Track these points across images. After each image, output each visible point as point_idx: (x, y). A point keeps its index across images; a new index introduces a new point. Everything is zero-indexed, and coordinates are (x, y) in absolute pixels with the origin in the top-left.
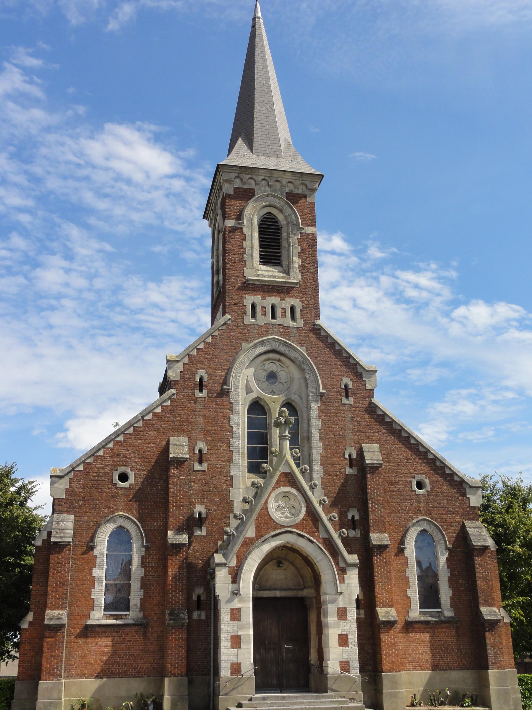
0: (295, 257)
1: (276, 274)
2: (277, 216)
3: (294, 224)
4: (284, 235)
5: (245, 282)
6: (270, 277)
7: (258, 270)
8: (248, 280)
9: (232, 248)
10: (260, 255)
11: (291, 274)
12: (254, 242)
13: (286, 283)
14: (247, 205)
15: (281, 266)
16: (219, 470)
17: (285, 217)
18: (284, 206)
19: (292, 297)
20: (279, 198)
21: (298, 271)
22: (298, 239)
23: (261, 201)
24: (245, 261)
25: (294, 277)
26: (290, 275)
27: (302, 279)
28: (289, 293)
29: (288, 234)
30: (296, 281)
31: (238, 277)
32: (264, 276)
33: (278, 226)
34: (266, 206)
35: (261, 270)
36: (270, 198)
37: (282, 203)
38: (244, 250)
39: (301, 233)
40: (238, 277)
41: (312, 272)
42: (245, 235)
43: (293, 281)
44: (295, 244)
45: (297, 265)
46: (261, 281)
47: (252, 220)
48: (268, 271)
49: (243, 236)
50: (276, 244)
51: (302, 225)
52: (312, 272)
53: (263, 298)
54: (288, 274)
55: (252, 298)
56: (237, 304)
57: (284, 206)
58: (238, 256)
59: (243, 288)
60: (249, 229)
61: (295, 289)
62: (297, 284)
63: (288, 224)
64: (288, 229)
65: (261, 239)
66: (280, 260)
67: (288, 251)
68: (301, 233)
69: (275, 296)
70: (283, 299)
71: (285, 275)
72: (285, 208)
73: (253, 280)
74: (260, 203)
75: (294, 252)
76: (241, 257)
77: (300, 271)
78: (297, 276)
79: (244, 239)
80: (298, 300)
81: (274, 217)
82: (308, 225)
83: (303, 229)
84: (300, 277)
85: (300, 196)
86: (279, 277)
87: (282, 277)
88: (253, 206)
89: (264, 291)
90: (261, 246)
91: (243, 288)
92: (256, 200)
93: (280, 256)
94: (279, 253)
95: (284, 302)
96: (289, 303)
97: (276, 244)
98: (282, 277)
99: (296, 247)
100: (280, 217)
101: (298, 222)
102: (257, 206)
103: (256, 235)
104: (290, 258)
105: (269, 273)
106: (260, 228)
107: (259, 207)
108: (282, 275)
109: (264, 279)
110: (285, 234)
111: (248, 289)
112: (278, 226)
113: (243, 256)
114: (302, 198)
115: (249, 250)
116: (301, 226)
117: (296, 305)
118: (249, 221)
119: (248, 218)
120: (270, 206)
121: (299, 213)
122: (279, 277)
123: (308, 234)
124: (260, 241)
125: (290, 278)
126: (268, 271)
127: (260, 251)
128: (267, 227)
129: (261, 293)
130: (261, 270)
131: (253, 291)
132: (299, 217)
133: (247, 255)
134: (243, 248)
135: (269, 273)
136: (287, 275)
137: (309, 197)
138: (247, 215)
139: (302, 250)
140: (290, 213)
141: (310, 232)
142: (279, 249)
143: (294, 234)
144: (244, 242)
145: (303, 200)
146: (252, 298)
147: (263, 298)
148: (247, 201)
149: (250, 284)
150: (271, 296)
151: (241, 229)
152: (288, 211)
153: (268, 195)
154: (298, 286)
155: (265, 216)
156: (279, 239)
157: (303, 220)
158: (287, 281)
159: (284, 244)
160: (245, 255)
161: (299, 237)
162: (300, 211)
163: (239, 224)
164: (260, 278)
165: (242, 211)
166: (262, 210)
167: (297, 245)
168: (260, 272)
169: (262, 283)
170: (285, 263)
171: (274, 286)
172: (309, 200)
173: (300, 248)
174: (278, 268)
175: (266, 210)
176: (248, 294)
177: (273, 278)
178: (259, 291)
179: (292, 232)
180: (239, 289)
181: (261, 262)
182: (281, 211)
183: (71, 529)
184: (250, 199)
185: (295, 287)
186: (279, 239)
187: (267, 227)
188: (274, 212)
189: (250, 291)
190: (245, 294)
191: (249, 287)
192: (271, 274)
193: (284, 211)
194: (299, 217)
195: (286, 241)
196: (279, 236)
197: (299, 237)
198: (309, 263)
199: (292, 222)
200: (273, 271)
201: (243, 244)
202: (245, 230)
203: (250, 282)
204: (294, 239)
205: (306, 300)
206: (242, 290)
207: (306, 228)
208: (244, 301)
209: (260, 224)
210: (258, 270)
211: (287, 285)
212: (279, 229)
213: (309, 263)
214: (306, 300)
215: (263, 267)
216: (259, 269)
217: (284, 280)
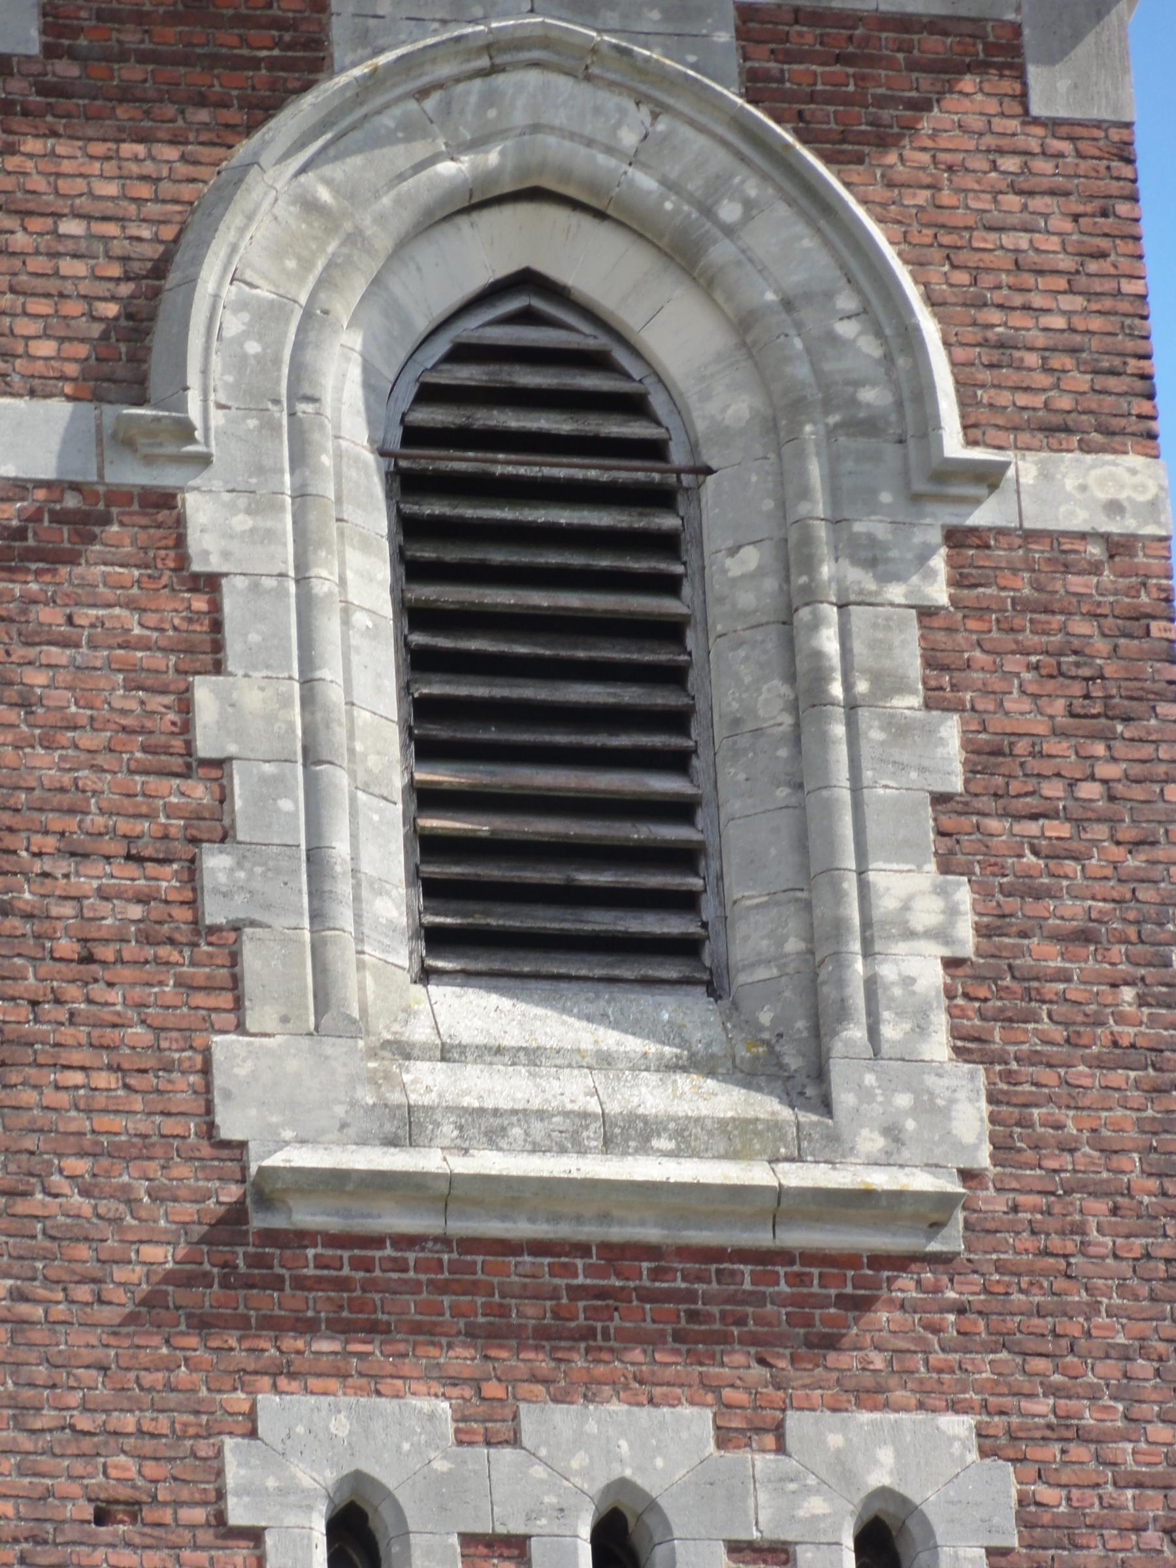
0: (903, 851)
1: (652, 1096)
2: (630, 318)
3: (866, 426)
4: (732, 569)
5: (236, 1215)
6: (572, 1130)
7: (404, 1051)
8: (267, 1190)
9: (45, 765)
10: (429, 846)
11: (850, 1083)
12: (330, 673)
13: (781, 1205)
14: (225, 194)
15: (714, 987)
16: (156, 990)
17: (744, 325)
18: (719, 186)
19: (870, 1395)
20: (648, 88)
21: (938, 1046)
22: (926, 613)
23: (410, 131)
24: (228, 941)
25: (893, 1133)
26: (844, 1099)
27: (1001, 1148)
28: (831, 1343)
29: (792, 557)
30: (922, 1182)
31: (140, 1149)
32: (489, 1126)
33: (655, 450)
34: (478, 201)
35: (447, 1053)
36: (523, 86)
37: (698, 152)
38: (199, 792)
39: (956, 538)
40: (140, 1149)
41: (1121, 1054)
42: (210, 583)
43: (881, 1180)
44: (888, 684)
45: (919, 968)
46: (447, 1193)
47: (302, 390)
48: (531, 1057)
49: (177, 609)
50: (629, 695)
51: (972, 431)
52: (1121, 1054)
53: (489, 1427)
54: (811, 1086)
55: (340, 1426)
56: (133, 1509)
57: (719, 186)
58: (125, 875)
59: (209, 1297)
60: (261, 504)
61: (906, 1286)
62: (932, 1211)
63: (778, 426)
64: (787, 489)
65: (430, 641)
66: (687, 902)
67: (802, 779)
68: (956, 538)
69: (648, 1391)
70: (752, 1428)
71: (766, 1106)
72: (729, 212)
73: (335, 1182)
74: (400, 156)
75: (883, 789)
76: (167, 880)
77: (968, 1046)
78: (932, 1110)
79: (209, 650)
80: (959, 1426)
81: (587, 338)
82: (1054, 430)
83: (989, 477)
84: (971, 1124)
85: (934, 45)
86: (687, 1137)
87: (736, 1138)
88: (310, 206)
89: (491, 1333)
90: (432, 728)
91: (209, 1297)
92: (342, 131)
93: (686, 857)
94: (681, 810)
95: (763, 1462)
96: (843, 1471)
97: (629, 695)
98: (736, 1138)
99: (899, 729)
100: (675, 335)
101: (921, 393)
102: (350, 194)
103: (363, 579)
104: (832, 871)
105: (551, 1090)
106: (405, 483)
107: (384, 216)
108: (723, 1100)
109: (488, 1162)
110: (750, 558)
111: (270, 1301)
112: (655, 450)
113: (192, 871)
114: (949, 69)
115: (278, 784)
116: (953, 444)
117: (927, 1495)
118: (253, 397)
119: (240, 362)
120: (535, 195)
121: (917, 265)
122: (687, 1137)
123: (1058, 549)
124: (418, 662)
125: (834, 1148)
126: (531, 1057)
127: (426, 798)
128: (504, 465)
129: (461, 1358)
130: (447, 1053)
131: (342, 1328)
132: (930, 328)
133: (247, 854)
134: (193, 765)
135: (551, 1090)
136: (793, 1098)
137: (1051, 59)
138: (233, 324)
139: (984, 755)
140: (795, 278)
141: (1079, 520)
142: (678, 762)
143: (872, 557)
144: (204, 691)
145: (972, 101)
146: (340, 1426)
147: (489, 1427)
148: (226, 136)
149: (303, 1238)
150: (589, 1391)
151: (162, 503)
152: (776, 249)
153: (497, 56)
154: (951, 1240)
155: (472, 329)
156: (671, 631)
157: (988, 361)
158: (796, 1176)
159: (735, 685)
160: (216, 863)
161: (939, 593)
162: (937, 241)
163: (125, 441)
164: (428, 1160)
165: (160, 269)
166: (426, 253)
167: (909, 703)
168: (426, 1082)
169: (460, 1227)
170: (755, 937)
171: (618, 1254)
172: (1051, 91)
173: (951, 730)
174: (667, 1008)
175: (486, 251)
176: (285, 1372)
177: (609, 1144)
178: (426, 1330)
179: (836, 522)
180: (151, 1309)
181: (436, 939)
182: (681, 253)
183: (101, 475)
184: (262, 109)
185: (901, 1262)
186: (671, 631)
187: (504, 465)
188: (593, 264)
189: (308, 1327)
190: (242, 1378)
191: (298, 1276)
192: (573, 1091)
193: (721, 252)
194: (930, 328)
195: (771, 640)
196: (670, 585)
197: (939, 593)
198: (1084, 937)
199: (834, 394)
200: (605, 1061)
201: (186, 706)
202: (212, 524)
203: (306, 1216)
204: (877, 619)
205: (1064, 1430)
206: (203, 1324)
207: (1025, 468)
208: (234, 1474)
209: (414, 436)
210: (404, 1051)
211: (795, 1238)
212: (662, 497)
213: (1084, 937)
214: (1064, 1430)
215: (472, 1011)
216: (420, 1032)
217: (758, 1174)
